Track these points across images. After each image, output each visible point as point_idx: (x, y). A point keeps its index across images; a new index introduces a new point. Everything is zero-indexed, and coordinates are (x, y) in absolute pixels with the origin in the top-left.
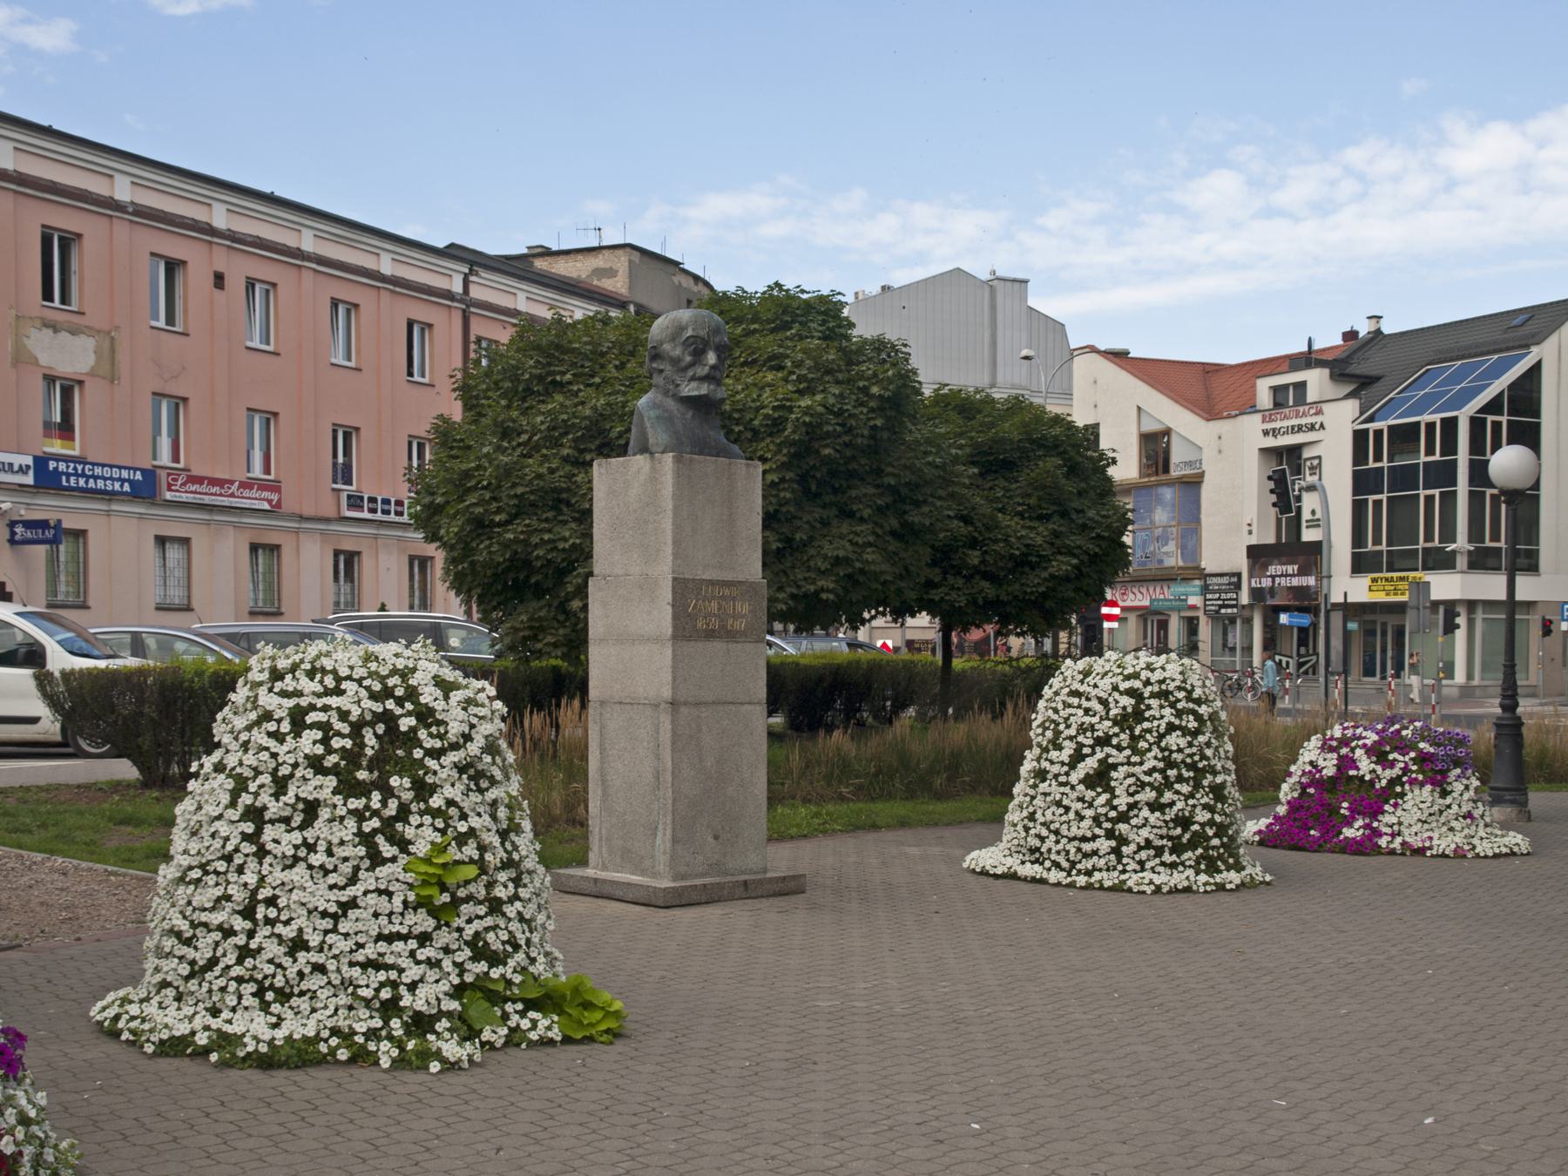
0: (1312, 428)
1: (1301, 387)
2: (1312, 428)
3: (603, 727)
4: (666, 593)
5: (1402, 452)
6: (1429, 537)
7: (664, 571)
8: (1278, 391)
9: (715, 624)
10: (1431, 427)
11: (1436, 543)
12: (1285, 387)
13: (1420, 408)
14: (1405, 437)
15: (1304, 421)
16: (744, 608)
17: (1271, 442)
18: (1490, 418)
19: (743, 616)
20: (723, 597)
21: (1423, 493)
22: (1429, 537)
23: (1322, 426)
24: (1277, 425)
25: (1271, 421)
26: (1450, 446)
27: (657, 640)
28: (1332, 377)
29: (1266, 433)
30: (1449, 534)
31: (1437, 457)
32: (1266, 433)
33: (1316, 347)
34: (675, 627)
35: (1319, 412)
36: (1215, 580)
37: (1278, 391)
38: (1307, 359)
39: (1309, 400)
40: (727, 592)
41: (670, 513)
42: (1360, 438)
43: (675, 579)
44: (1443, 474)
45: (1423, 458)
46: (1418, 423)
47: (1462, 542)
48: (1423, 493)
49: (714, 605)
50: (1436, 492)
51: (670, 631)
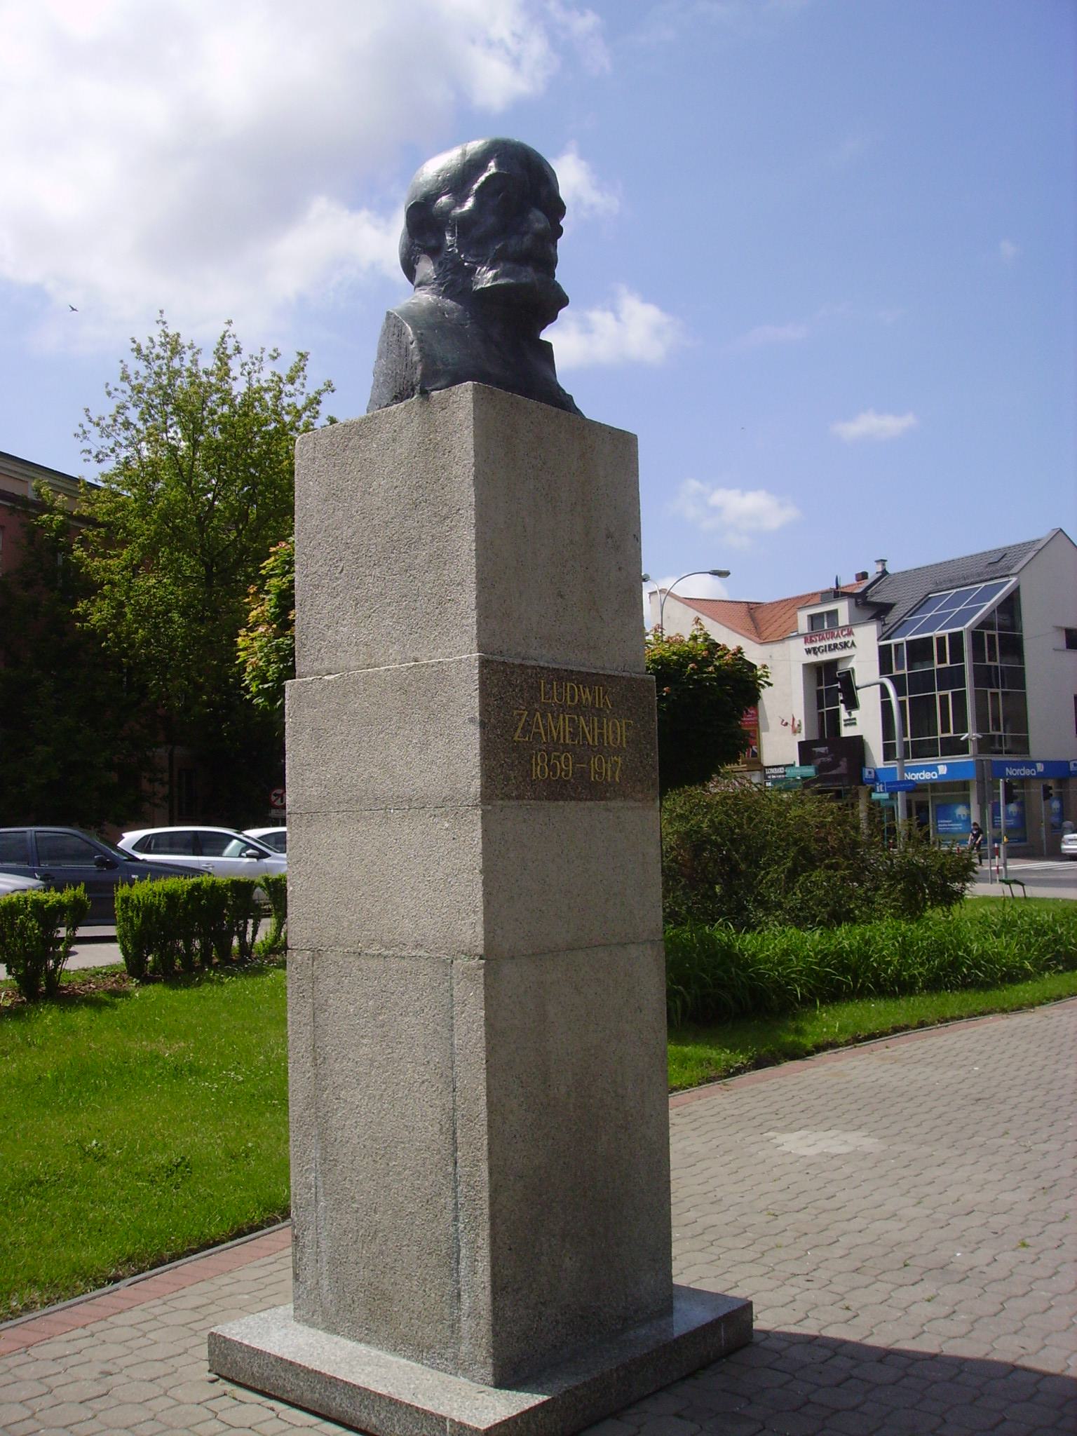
0: (845, 645)
1: (833, 614)
2: (845, 645)
3: (317, 1009)
4: (466, 699)
5: (918, 664)
6: (945, 729)
7: (460, 655)
8: (812, 618)
9: (566, 765)
10: (941, 640)
11: (951, 734)
12: (821, 615)
13: (931, 625)
14: (919, 650)
15: (838, 641)
16: (617, 730)
17: (813, 658)
18: (986, 632)
19: (618, 751)
20: (579, 708)
21: (938, 694)
22: (945, 729)
23: (853, 644)
24: (817, 645)
25: (812, 641)
26: (957, 655)
27: (446, 805)
28: (857, 604)
29: (808, 651)
30: (961, 727)
31: (948, 664)
32: (808, 651)
33: (842, 584)
34: (488, 775)
35: (850, 633)
36: (772, 771)
37: (812, 618)
38: (837, 594)
39: (840, 624)
40: (587, 696)
41: (470, 515)
42: (884, 653)
43: (484, 664)
44: (953, 678)
45: (937, 666)
46: (931, 638)
47: (971, 734)
48: (938, 694)
49: (564, 724)
50: (949, 693)
51: (476, 786)
